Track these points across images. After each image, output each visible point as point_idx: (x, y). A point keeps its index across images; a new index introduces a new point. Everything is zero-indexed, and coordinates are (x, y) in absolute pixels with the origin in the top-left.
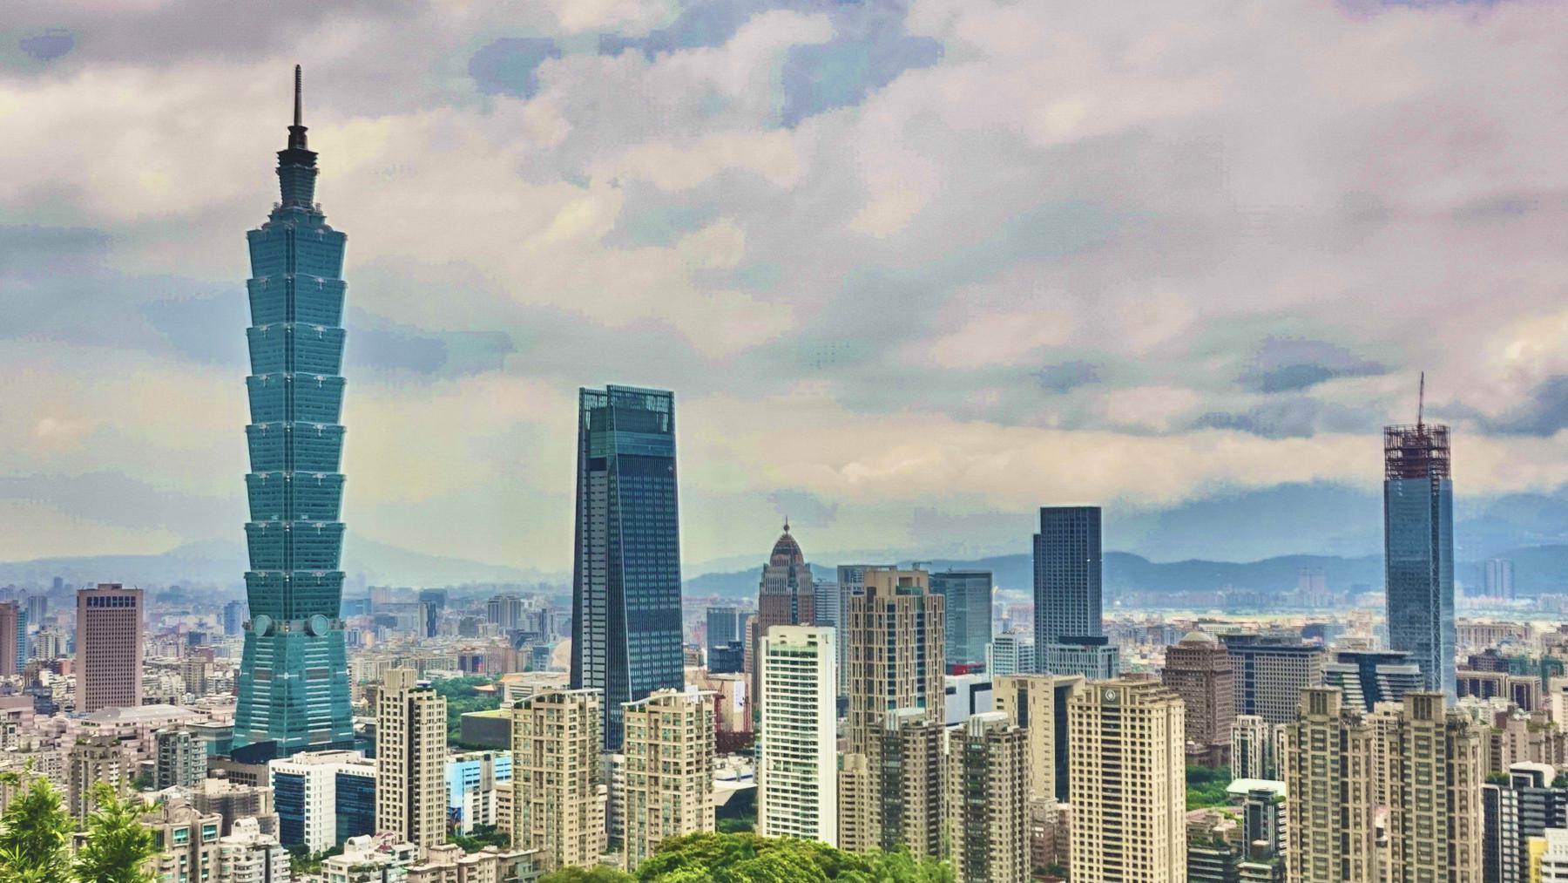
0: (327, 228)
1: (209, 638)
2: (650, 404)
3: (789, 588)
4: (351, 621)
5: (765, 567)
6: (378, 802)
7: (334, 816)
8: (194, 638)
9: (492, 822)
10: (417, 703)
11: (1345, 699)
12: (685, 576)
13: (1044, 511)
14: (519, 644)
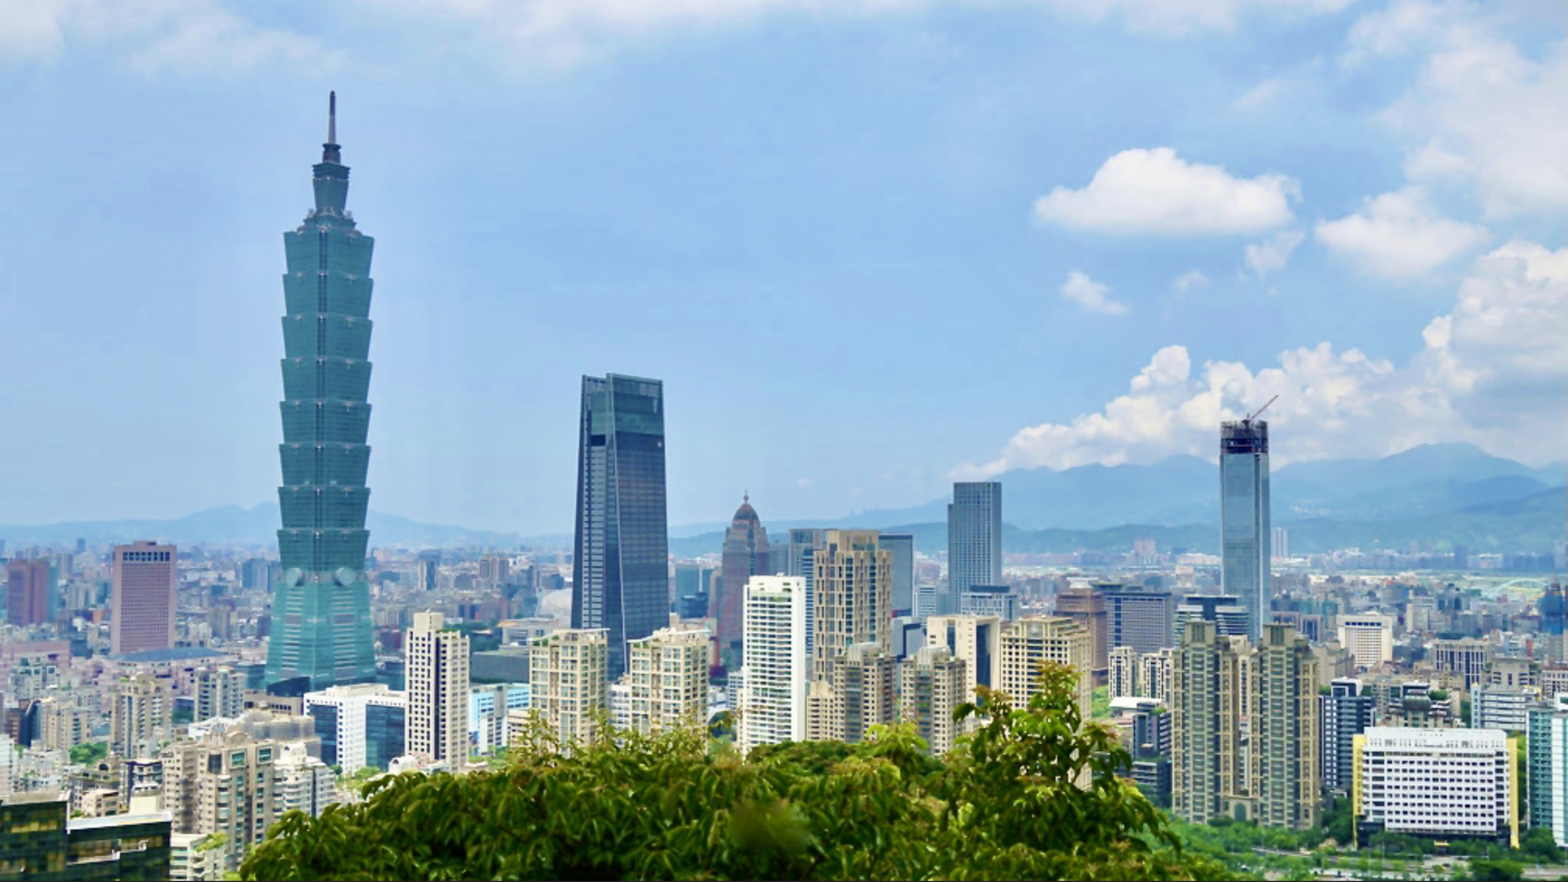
0: (359, 233)
1: (230, 591)
2: (643, 392)
3: (750, 548)
4: (371, 573)
5: (728, 531)
6: (407, 728)
7: (364, 742)
8: (217, 591)
9: (504, 744)
10: (443, 642)
11: (1218, 631)
12: (671, 534)
13: (957, 486)
14: (511, 595)
